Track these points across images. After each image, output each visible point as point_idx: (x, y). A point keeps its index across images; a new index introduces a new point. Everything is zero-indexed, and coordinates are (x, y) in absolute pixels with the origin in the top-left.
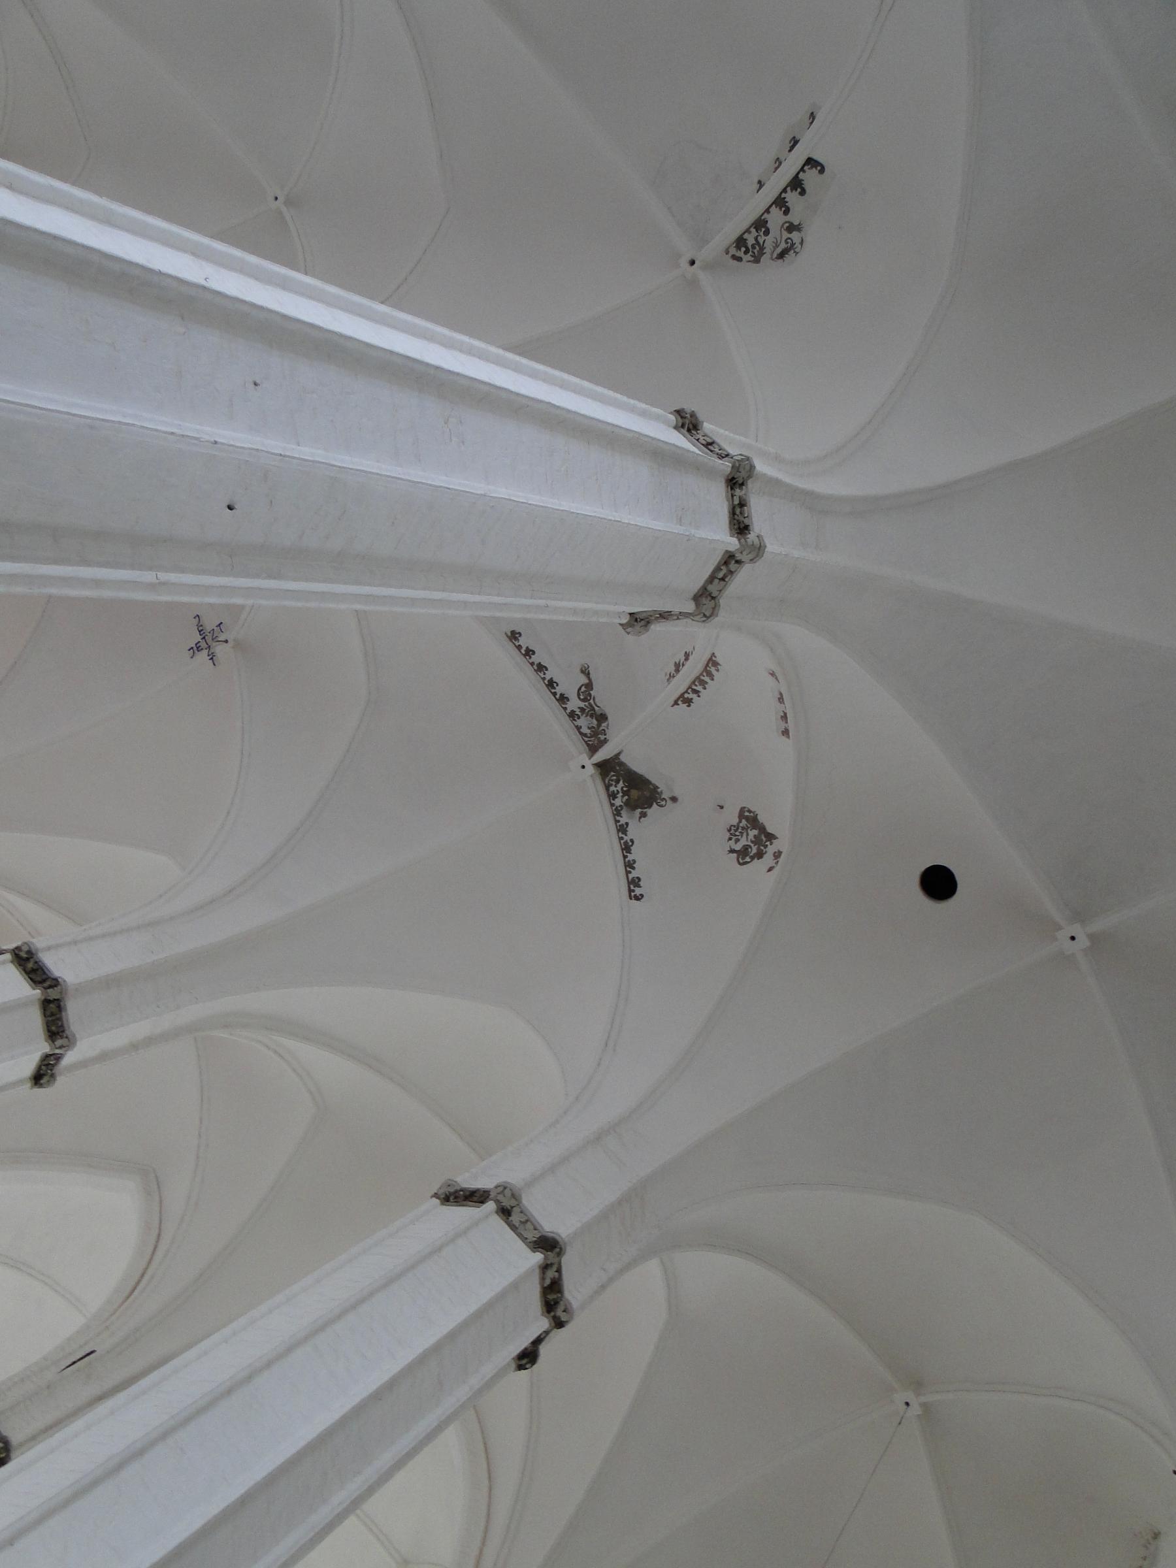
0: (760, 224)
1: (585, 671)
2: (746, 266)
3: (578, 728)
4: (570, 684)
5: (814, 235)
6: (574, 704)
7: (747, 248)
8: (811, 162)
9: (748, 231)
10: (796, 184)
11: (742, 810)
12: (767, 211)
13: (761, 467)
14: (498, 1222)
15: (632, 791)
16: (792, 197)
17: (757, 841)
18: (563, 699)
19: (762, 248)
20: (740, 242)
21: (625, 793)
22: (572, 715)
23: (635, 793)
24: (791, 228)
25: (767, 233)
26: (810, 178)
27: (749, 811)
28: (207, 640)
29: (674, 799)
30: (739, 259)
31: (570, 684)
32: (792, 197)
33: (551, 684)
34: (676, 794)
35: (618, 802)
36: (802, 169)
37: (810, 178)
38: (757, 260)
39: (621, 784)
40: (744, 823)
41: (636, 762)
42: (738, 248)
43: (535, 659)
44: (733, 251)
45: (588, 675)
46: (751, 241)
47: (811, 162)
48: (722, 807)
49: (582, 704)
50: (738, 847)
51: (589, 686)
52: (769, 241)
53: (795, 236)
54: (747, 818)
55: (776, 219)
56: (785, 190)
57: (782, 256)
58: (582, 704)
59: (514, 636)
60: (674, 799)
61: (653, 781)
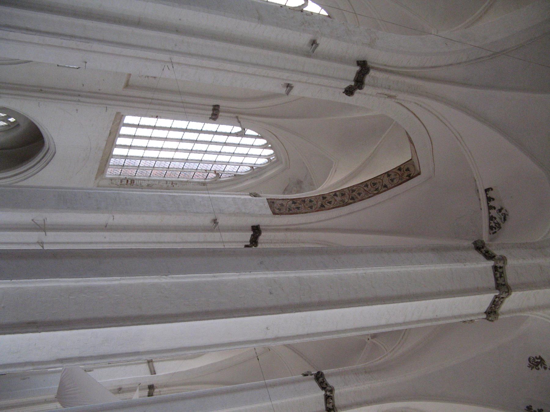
0: (491, 218)
8: (487, 190)
9: (490, 223)
10: (489, 199)
12: (490, 213)
13: (325, 372)
16: (492, 203)
19: (498, 223)
20: (491, 228)
24: (500, 210)
25: (495, 218)
30: (495, 232)
32: (492, 203)
42: (492, 230)
44: (492, 232)
46: (493, 225)
47: (487, 190)
52: (498, 220)
53: (503, 211)
55: (494, 213)
56: (488, 204)
57: (505, 220)
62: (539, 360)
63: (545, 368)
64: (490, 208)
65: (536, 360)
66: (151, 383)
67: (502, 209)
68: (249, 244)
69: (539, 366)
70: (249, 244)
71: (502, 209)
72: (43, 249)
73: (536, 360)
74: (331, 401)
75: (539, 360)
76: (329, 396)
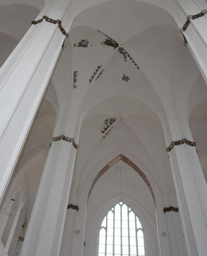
0: (111, 124)
1: (126, 60)
2: (113, 118)
3: (125, 51)
4: (128, 58)
5: (103, 123)
6: (127, 55)
7: (113, 121)
8: (103, 132)
9: (113, 123)
10: (106, 129)
11: (87, 46)
12: (110, 125)
14: (64, 141)
15: (110, 43)
16: (107, 127)
17: (82, 44)
18: (129, 56)
19: (111, 120)
20: (114, 121)
21: (112, 41)
22: (127, 53)
23: (110, 42)
24: (106, 123)
25: (110, 123)
26: (104, 130)
27: (86, 47)
28: (112, 128)
29: (102, 44)
30: (114, 119)
31: (128, 58)
32: (107, 127)
33: (131, 59)
34: (102, 44)
35: (112, 40)
36: (105, 131)
37: (104, 130)
38: (111, 119)
39: (113, 43)
40: (86, 45)
41: (111, 48)
42: (114, 120)
43: (135, 64)
44: (115, 120)
45: (125, 60)
46: (112, 121)
47: (103, 132)
48: (91, 45)
49: (125, 54)
50: (85, 41)
51: (125, 58)
52: (110, 121)
53: (106, 122)
54: (86, 45)
55: (109, 124)
56: (107, 128)
57: (107, 120)
58: (125, 54)
59: (138, 68)
60: (102, 44)
61: (107, 45)
62: (124, 79)
63: (124, 75)
64: (108, 127)
65: (125, 79)
66: (24, 240)
67: (105, 123)
68: (76, 210)
69: (126, 77)
70: (76, 210)
71: (105, 123)
72: (101, 228)
73: (125, 79)
74: (170, 147)
75: (124, 79)
76: (169, 149)
